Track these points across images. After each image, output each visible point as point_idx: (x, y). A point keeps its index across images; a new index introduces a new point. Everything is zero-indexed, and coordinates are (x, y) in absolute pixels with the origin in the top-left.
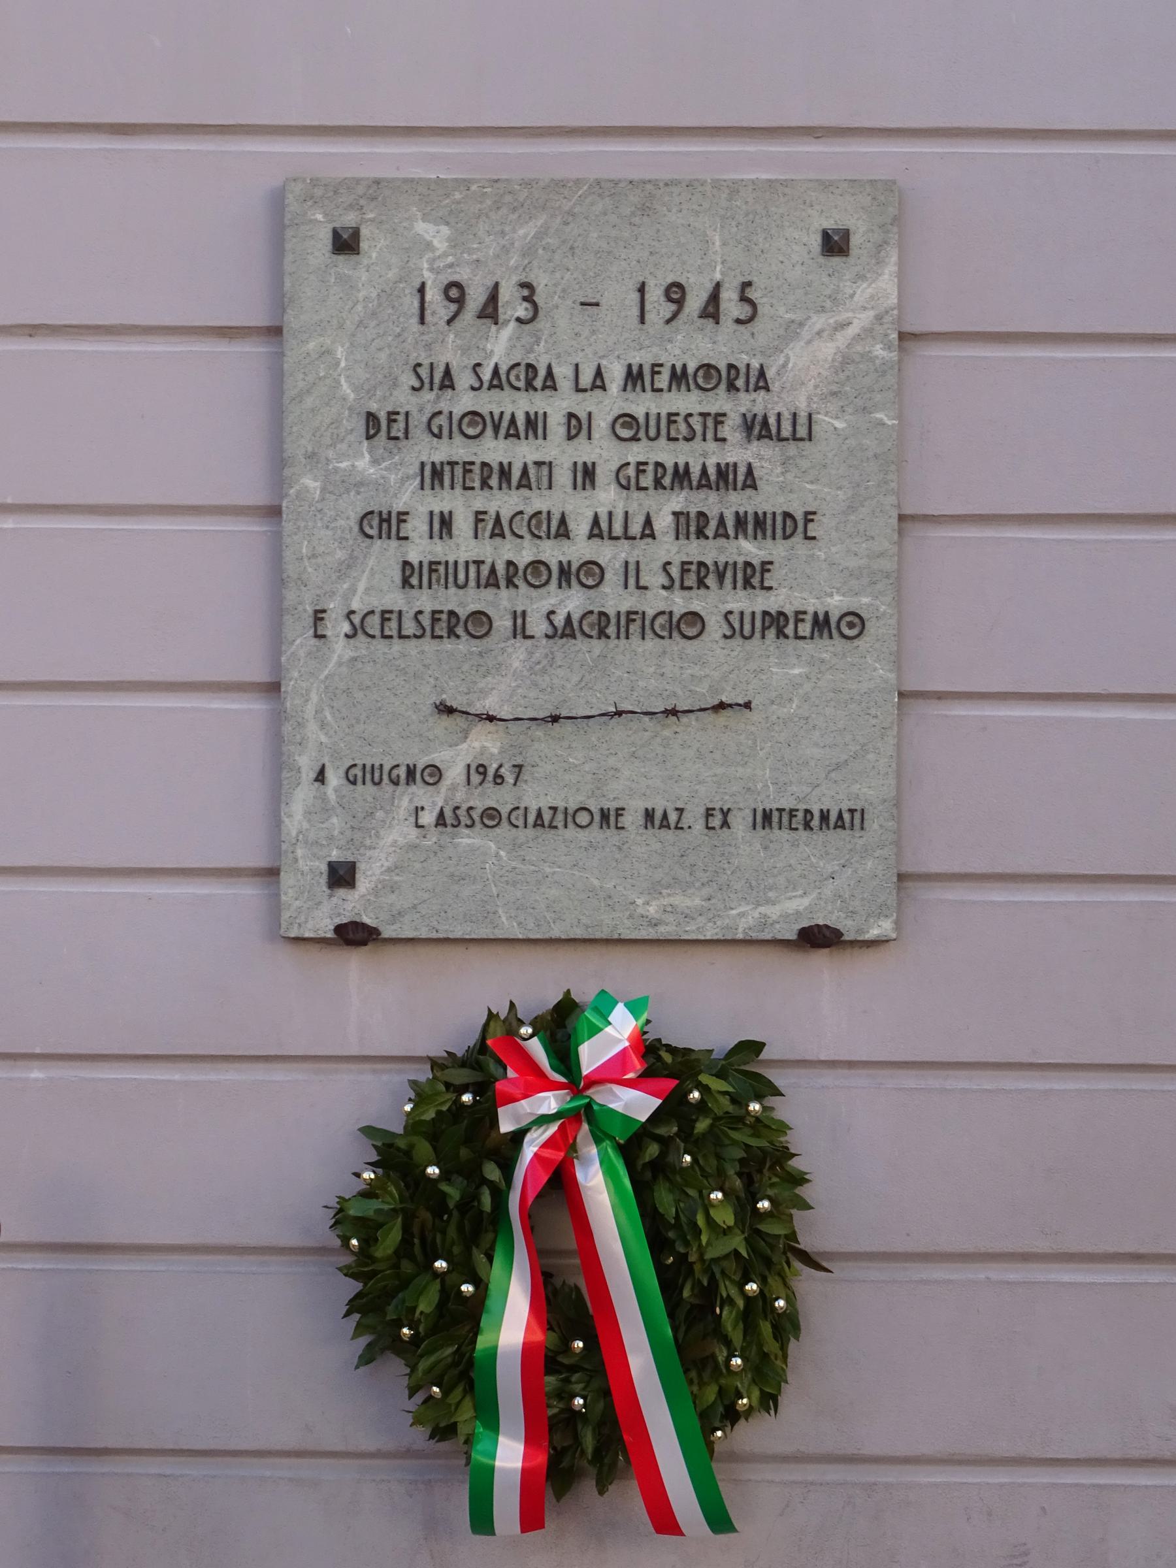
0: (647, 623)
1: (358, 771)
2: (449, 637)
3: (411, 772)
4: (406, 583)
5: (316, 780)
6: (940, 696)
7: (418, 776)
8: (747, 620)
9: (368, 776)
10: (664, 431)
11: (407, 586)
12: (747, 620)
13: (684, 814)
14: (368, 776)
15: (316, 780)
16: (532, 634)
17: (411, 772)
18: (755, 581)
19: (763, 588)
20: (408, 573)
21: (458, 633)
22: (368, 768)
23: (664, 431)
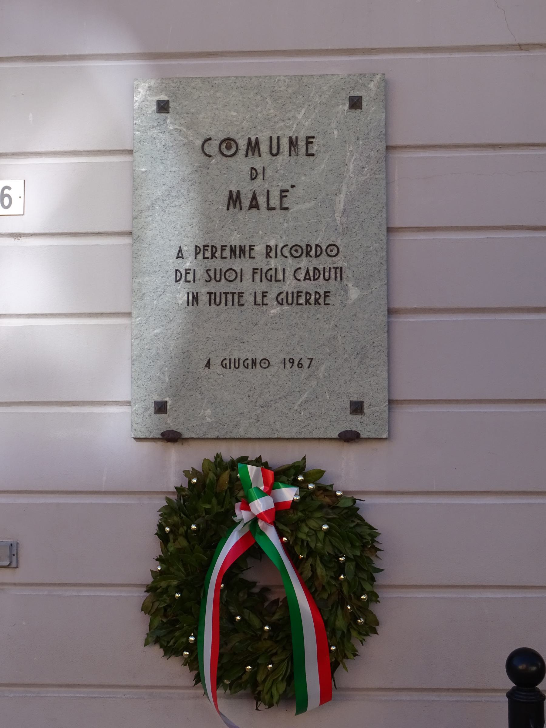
0: (223, 273)
1: (227, 362)
2: (306, 305)
3: (254, 362)
4: (268, 255)
5: (206, 366)
6: (410, 402)
7: (258, 364)
8: (290, 296)
9: (232, 365)
10: (295, 301)
11: (268, 256)
12: (290, 296)
13: (313, 362)
14: (232, 365)
15: (206, 366)
16: (308, 360)
17: (254, 362)
18: (321, 301)
19: (325, 304)
20: (269, 251)
21: (216, 256)
22: (233, 361)
23: (295, 301)
